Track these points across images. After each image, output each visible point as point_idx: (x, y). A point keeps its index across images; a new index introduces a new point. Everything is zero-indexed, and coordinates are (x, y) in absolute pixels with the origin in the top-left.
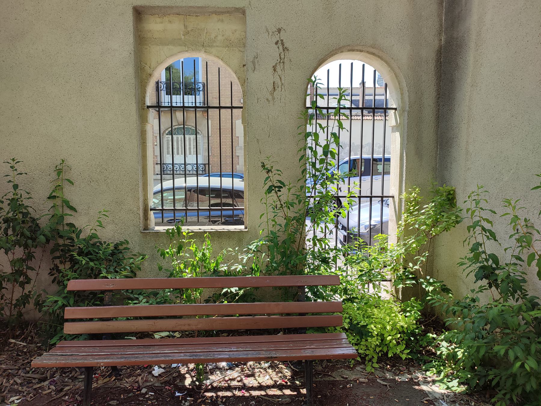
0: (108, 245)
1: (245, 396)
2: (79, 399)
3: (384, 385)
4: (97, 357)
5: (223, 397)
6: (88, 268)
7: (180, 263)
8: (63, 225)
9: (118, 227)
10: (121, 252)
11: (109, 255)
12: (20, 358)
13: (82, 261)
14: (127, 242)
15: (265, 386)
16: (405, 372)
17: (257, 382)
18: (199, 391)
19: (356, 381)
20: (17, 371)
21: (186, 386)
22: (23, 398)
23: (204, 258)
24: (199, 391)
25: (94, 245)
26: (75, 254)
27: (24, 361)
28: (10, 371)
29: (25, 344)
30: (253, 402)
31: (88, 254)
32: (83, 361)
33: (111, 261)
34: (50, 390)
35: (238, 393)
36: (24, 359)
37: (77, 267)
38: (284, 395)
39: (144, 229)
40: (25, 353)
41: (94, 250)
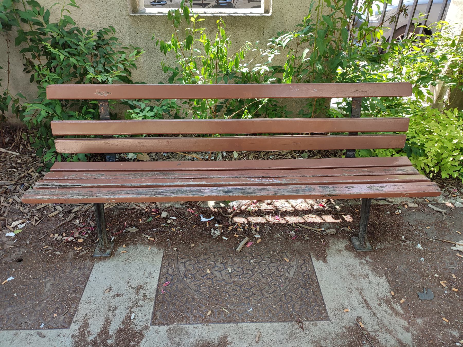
0: (89, 33)
1: (280, 224)
2: (92, 224)
3: (437, 211)
4: (105, 190)
5: (256, 224)
6: (69, 65)
7: (187, 62)
8: (24, 4)
9: (97, 8)
10: (108, 44)
11: (93, 49)
12: (15, 170)
13: (59, 55)
14: (114, 30)
15: (301, 211)
16: (457, 194)
17: (291, 206)
18: (227, 216)
19: (403, 206)
20: (14, 187)
21: (209, 208)
22: (27, 222)
23: (219, 56)
24: (227, 216)
25: (70, 33)
26: (48, 44)
27: (20, 174)
28: (7, 187)
29: (18, 154)
30: (293, 232)
31: (65, 46)
32: (88, 197)
33: (96, 55)
34: (57, 212)
35: (271, 219)
36: (19, 172)
37: (54, 64)
38: (325, 223)
39: (133, 11)
40: (20, 164)
41: (71, 41)
